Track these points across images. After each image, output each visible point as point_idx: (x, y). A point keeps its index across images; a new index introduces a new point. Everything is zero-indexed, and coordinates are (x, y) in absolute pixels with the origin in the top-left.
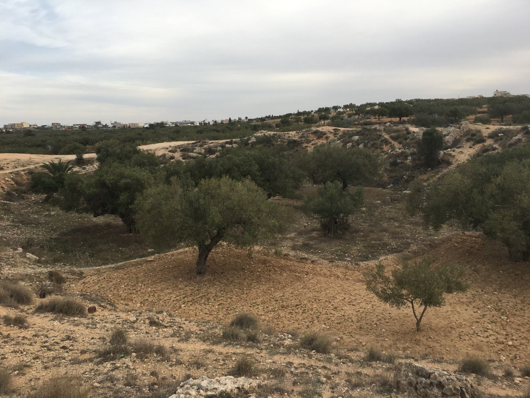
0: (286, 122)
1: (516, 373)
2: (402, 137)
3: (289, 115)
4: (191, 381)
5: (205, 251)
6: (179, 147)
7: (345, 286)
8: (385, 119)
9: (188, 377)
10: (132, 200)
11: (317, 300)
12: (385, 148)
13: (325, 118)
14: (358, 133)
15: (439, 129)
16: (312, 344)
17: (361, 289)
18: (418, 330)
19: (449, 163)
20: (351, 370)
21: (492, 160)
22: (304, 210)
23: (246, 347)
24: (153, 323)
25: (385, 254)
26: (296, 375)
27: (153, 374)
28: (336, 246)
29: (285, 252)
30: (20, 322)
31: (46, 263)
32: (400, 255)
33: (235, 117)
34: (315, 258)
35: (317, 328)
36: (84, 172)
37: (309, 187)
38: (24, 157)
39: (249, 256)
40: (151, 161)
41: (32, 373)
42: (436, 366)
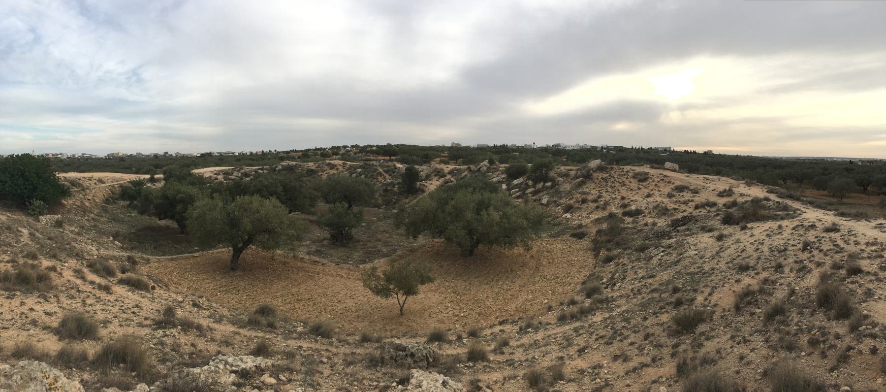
0: (306, 155)
1: (464, 335)
2: (391, 171)
3: (309, 150)
4: (220, 357)
5: (237, 252)
6: (222, 171)
7: (348, 284)
8: (380, 157)
9: (219, 353)
10: (185, 209)
11: (325, 295)
12: (380, 179)
13: (337, 154)
14: (360, 167)
15: (416, 167)
16: (319, 331)
17: (360, 285)
18: (402, 314)
19: (423, 191)
20: (348, 351)
21: (450, 189)
22: (319, 223)
23: (266, 332)
24: (195, 305)
25: (378, 258)
26: (304, 357)
27: (193, 345)
28: (341, 252)
29: (301, 256)
30: (107, 289)
31: (126, 249)
32: (389, 258)
33: (266, 150)
34: (325, 261)
35: (325, 318)
36: (154, 187)
37: (322, 206)
38: (118, 175)
39: (273, 258)
40: (200, 181)
41: (111, 328)
42: (413, 340)
